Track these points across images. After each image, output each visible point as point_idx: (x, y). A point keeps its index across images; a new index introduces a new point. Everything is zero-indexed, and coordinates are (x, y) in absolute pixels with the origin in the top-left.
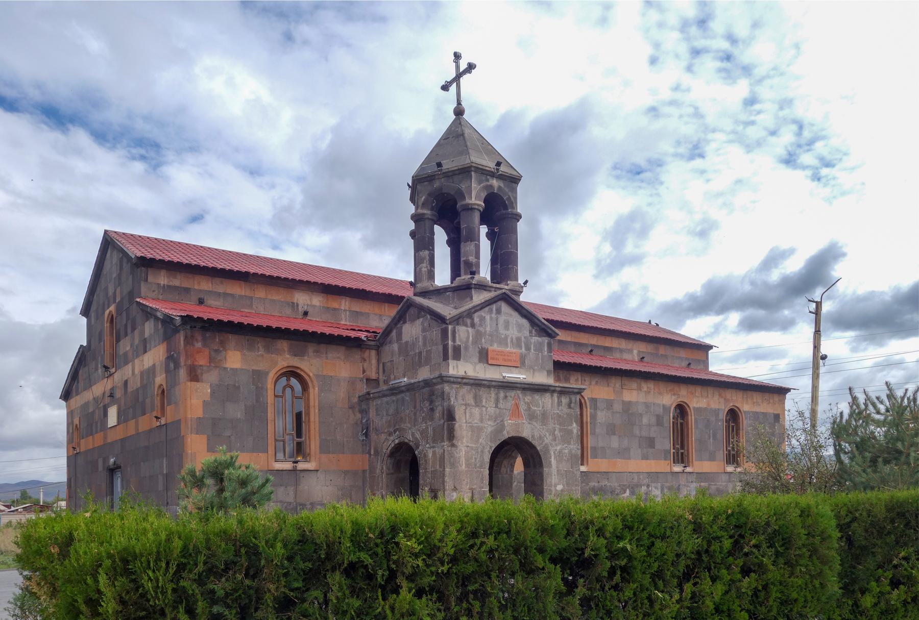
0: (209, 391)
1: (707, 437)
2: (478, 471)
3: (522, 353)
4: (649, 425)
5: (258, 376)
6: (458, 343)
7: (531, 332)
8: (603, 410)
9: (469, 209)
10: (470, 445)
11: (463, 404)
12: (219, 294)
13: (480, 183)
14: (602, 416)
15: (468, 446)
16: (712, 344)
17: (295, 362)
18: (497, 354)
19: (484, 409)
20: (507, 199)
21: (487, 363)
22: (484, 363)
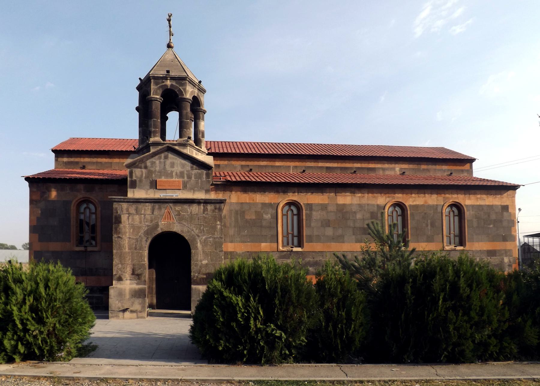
0: (40, 212)
1: (424, 225)
2: (137, 252)
3: (184, 181)
4: (363, 219)
5: (67, 204)
6: (134, 178)
7: (192, 167)
8: (318, 211)
9: (185, 100)
10: (131, 237)
11: (127, 214)
12: (94, 163)
13: (156, 84)
14: (316, 215)
15: (130, 238)
16: (475, 158)
17: (88, 195)
18: (164, 183)
19: (143, 216)
20: (178, 91)
21: (156, 189)
22: (154, 189)
